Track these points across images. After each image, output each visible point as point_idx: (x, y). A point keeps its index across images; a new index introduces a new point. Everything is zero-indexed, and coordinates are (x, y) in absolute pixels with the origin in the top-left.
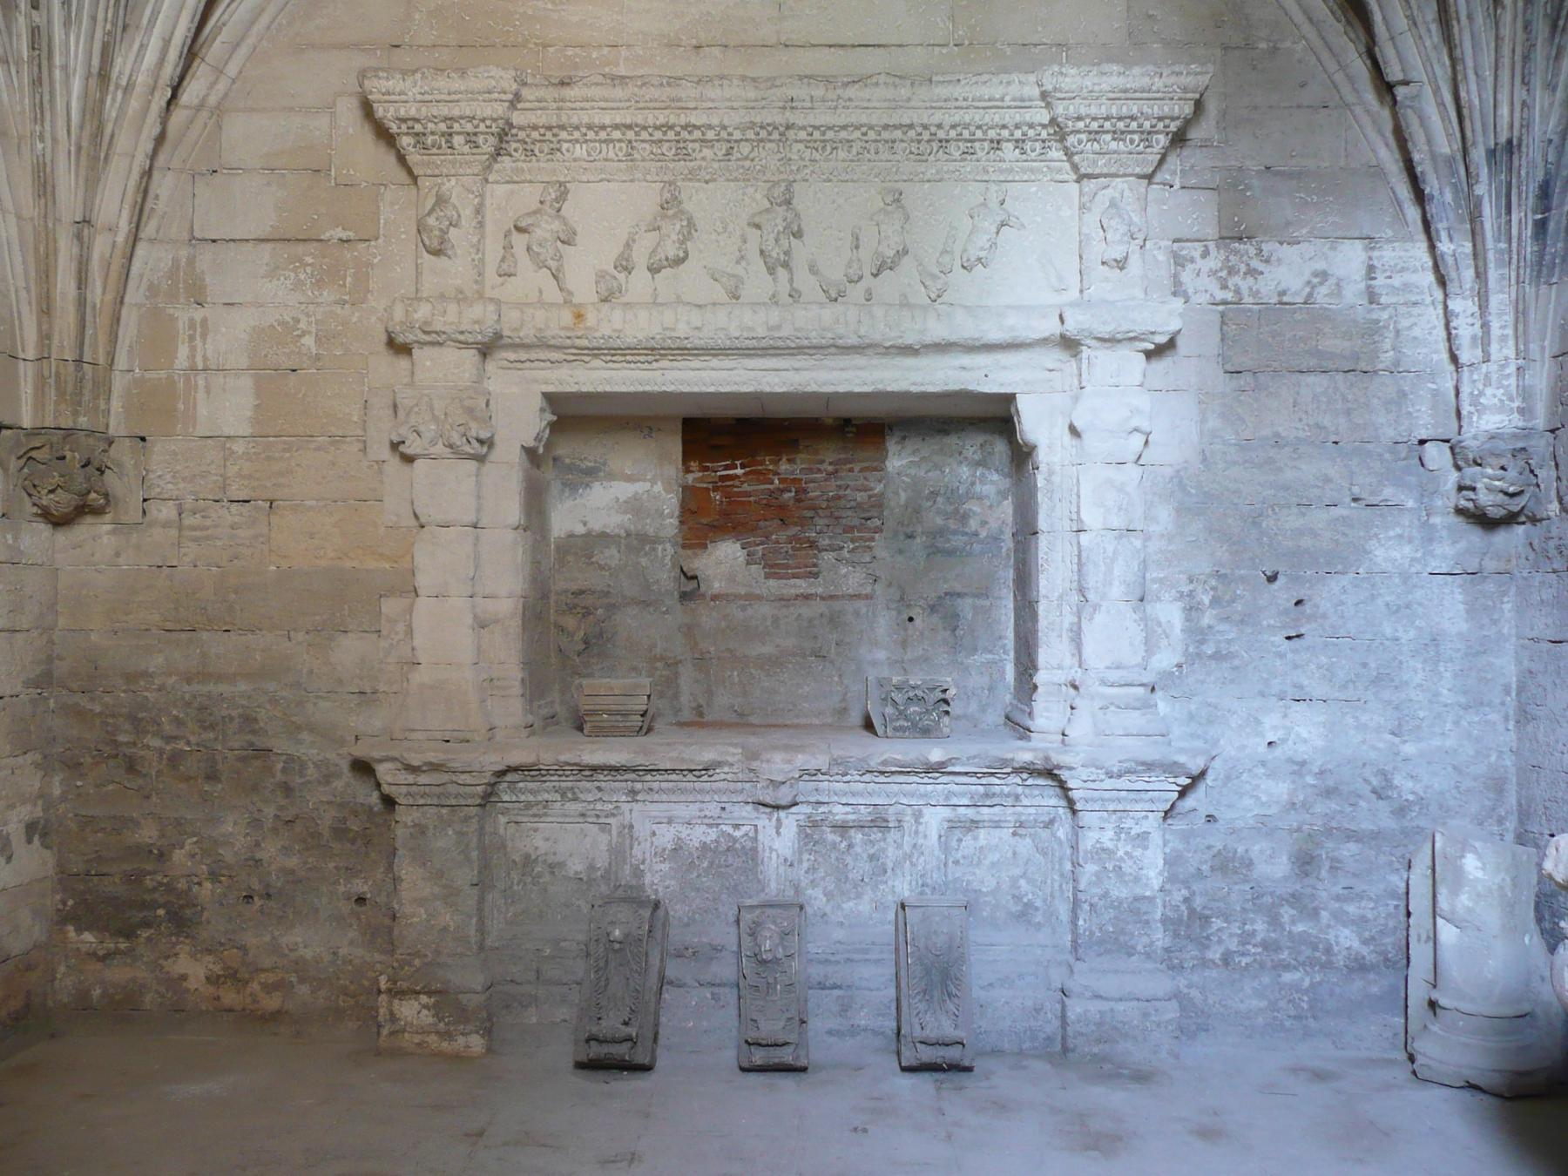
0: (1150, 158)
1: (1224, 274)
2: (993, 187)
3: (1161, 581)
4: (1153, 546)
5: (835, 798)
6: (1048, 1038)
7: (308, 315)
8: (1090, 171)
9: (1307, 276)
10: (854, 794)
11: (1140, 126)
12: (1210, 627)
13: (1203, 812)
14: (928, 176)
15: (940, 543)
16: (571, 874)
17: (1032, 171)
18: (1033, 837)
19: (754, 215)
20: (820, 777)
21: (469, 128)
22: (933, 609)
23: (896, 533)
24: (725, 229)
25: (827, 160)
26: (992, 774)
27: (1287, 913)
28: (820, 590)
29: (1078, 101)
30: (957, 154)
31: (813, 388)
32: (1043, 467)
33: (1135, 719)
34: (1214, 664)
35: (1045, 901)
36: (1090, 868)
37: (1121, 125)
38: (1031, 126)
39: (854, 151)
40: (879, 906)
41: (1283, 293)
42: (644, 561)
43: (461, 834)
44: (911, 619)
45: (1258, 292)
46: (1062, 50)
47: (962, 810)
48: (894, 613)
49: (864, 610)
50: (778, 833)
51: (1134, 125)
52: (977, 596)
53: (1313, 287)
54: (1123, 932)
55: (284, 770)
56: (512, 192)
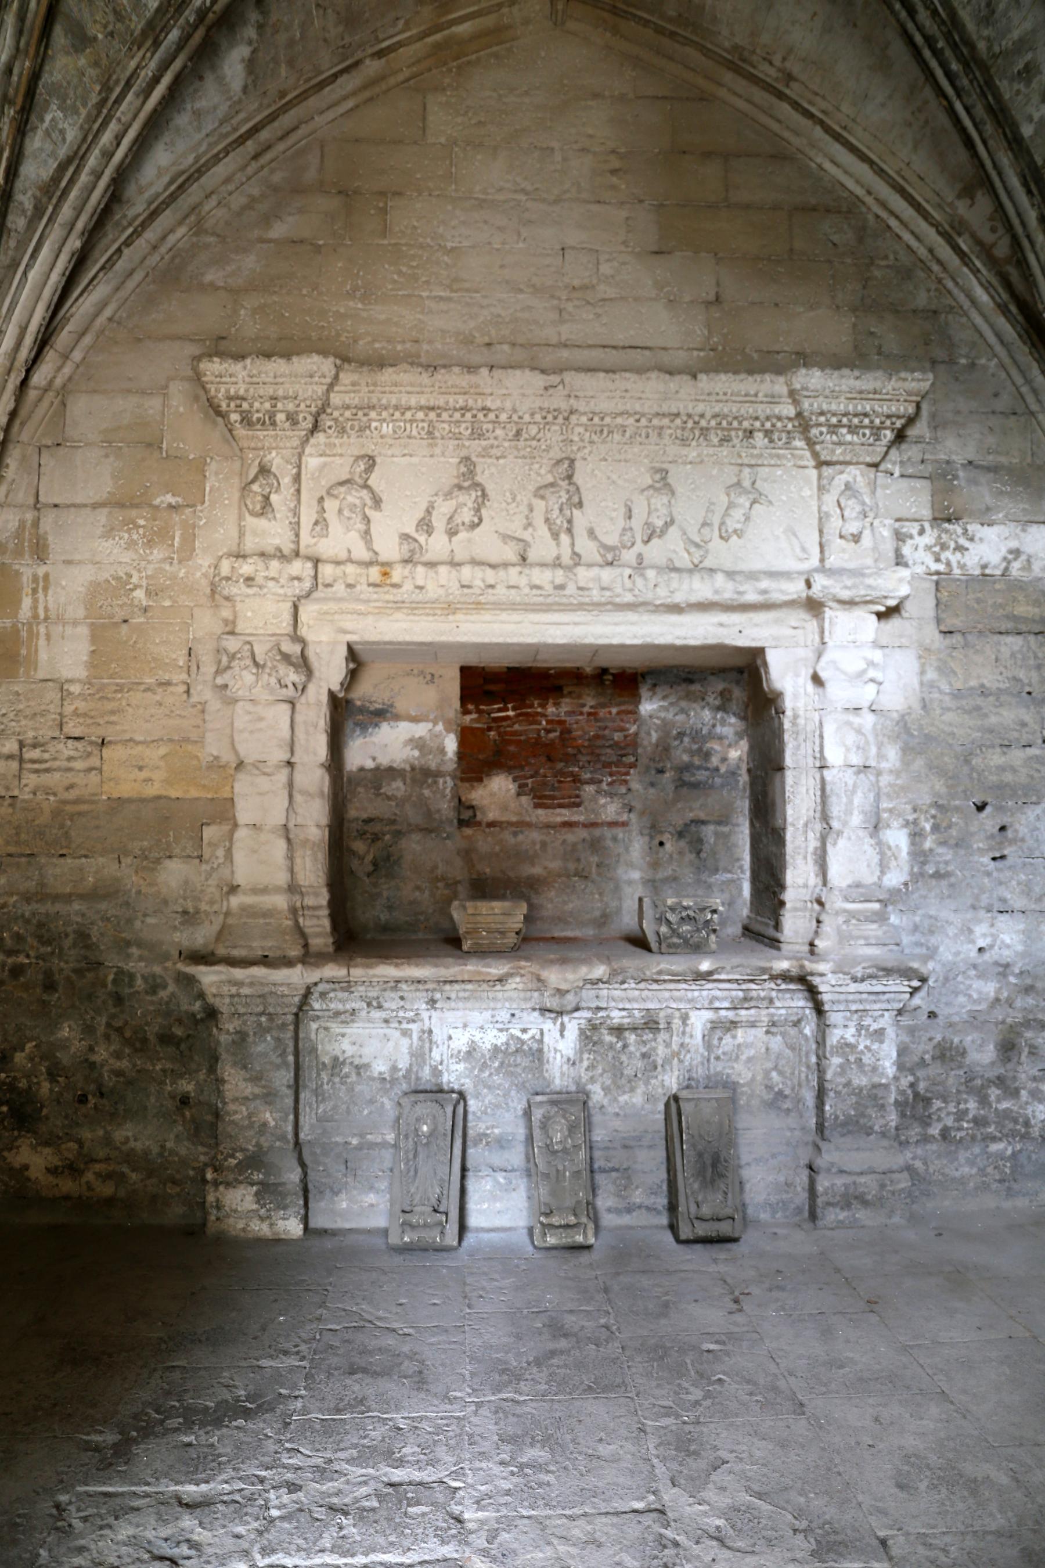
0: (878, 449)
1: (937, 549)
2: (747, 471)
3: (890, 811)
4: (885, 780)
5: (612, 1004)
6: (798, 1208)
7: (139, 571)
8: (828, 458)
9: (1003, 551)
10: (629, 1001)
11: (872, 422)
12: (931, 850)
13: (926, 1008)
14: (690, 458)
15: (687, 777)
16: (376, 1075)
17: (778, 456)
18: (783, 1034)
19: (540, 488)
20: (601, 985)
21: (291, 407)
22: (680, 835)
23: (648, 768)
24: (514, 499)
25: (604, 442)
26: (752, 981)
27: (994, 1092)
28: (582, 818)
29: (821, 399)
30: (715, 440)
31: (590, 640)
32: (789, 713)
33: (873, 929)
34: (934, 882)
35: (793, 1089)
36: (836, 1061)
37: (856, 421)
38: (779, 418)
39: (628, 435)
40: (649, 1098)
41: (984, 567)
42: (426, 792)
43: (278, 1040)
44: (661, 844)
45: (965, 565)
46: (803, 359)
47: (723, 1013)
48: (647, 838)
49: (621, 836)
50: (562, 1035)
51: (866, 421)
52: (719, 823)
53: (1009, 562)
54: (863, 1115)
55: (114, 981)
56: (325, 465)
